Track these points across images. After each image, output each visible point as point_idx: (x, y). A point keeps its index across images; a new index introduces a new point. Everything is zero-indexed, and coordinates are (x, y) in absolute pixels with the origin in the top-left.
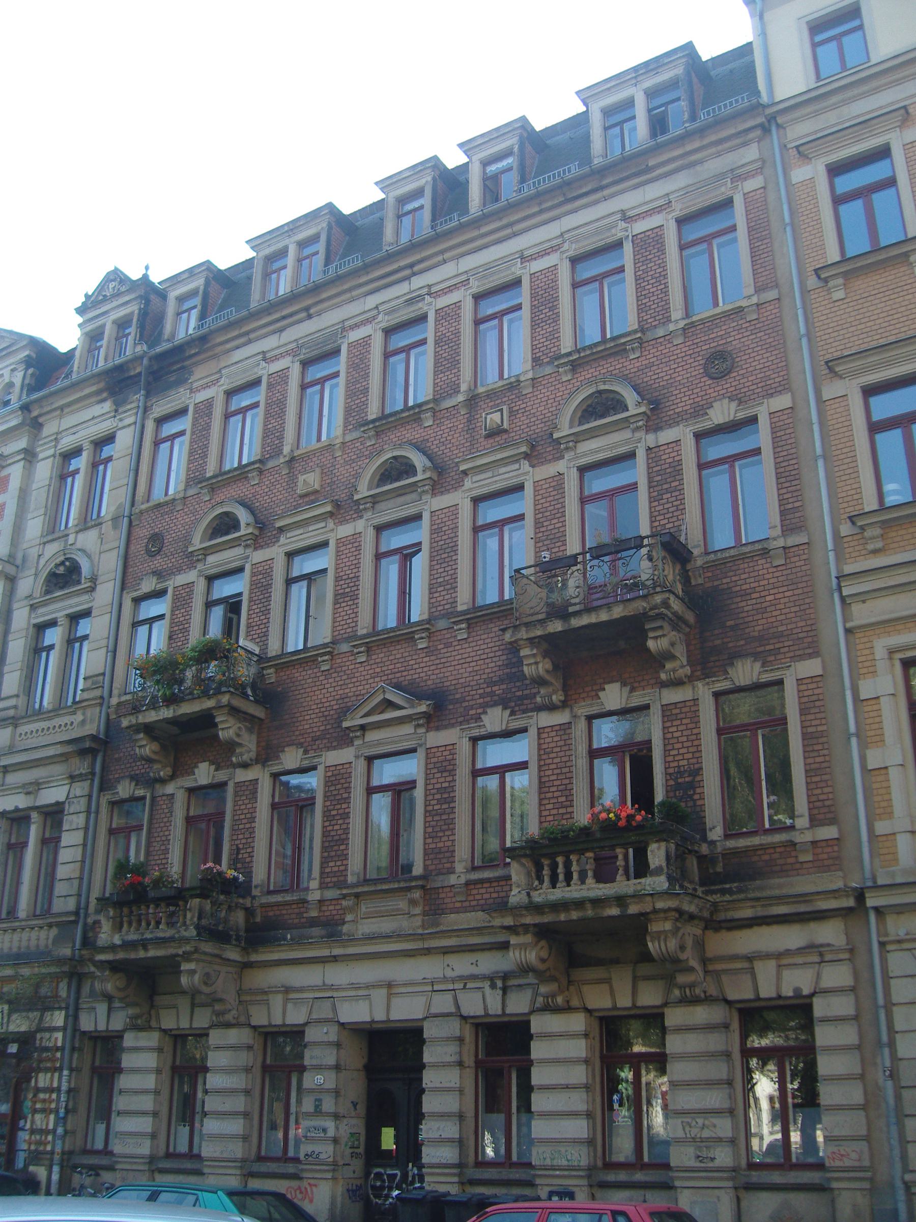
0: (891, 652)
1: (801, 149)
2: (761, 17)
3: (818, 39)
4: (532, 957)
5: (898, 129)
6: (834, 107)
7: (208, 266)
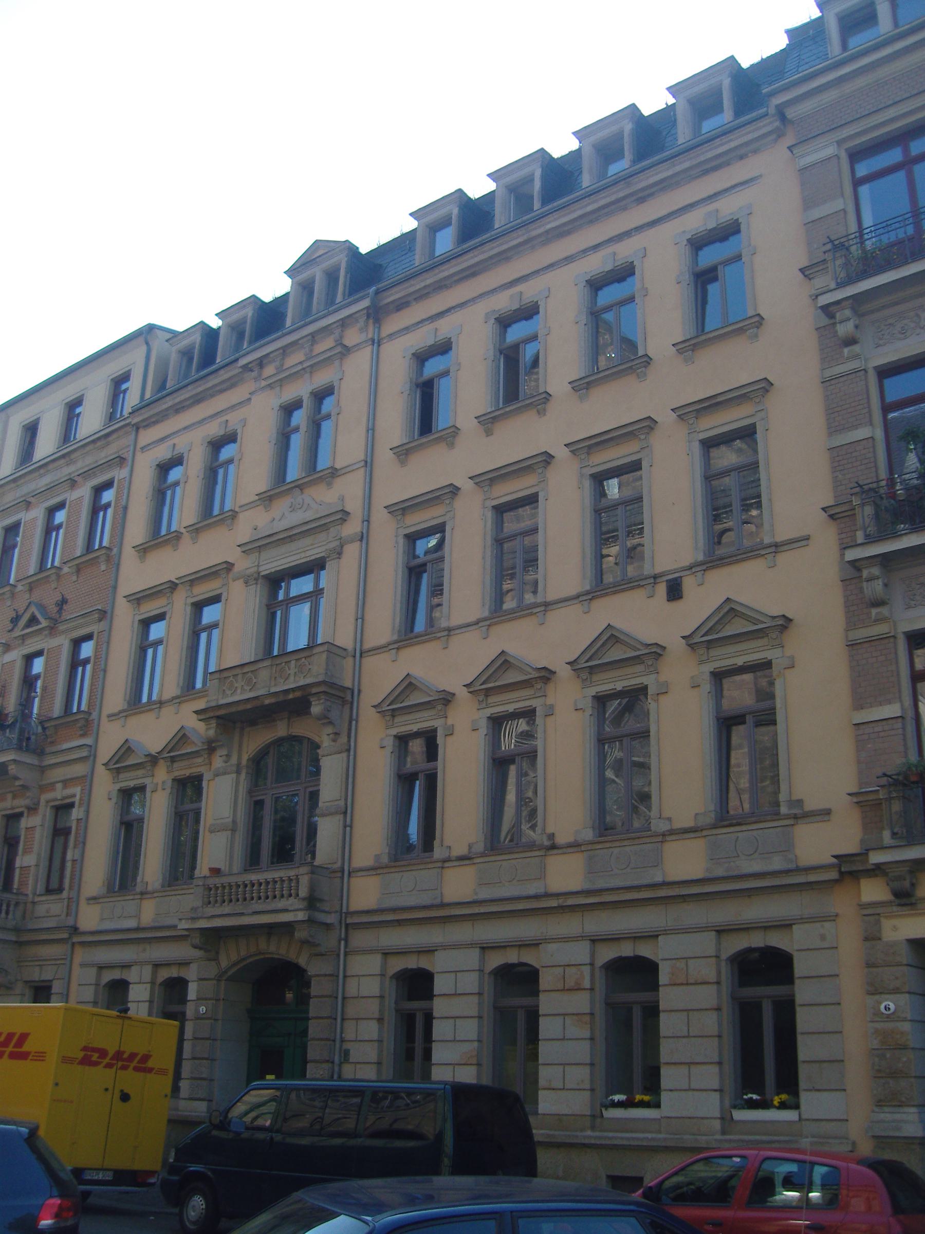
7: (254, 299)
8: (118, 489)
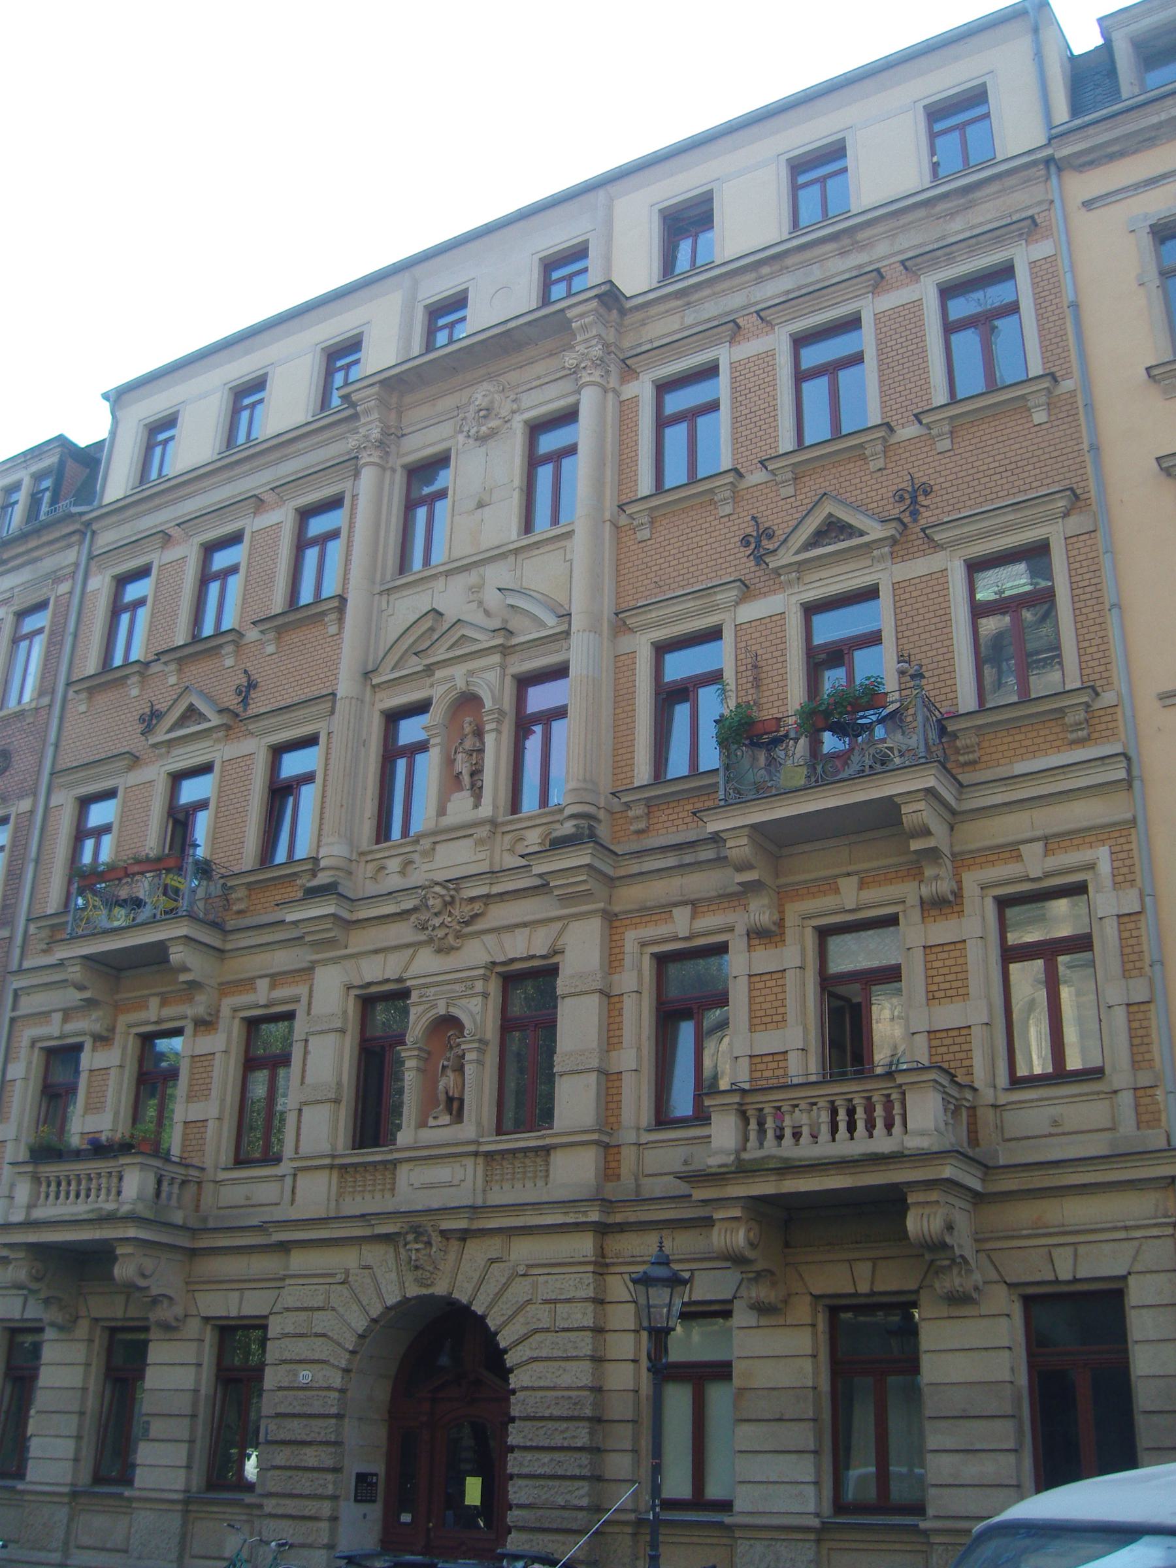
3: (938, 127)
4: (739, 1238)
5: (870, 295)
7: (62, 442)
8: (158, 579)
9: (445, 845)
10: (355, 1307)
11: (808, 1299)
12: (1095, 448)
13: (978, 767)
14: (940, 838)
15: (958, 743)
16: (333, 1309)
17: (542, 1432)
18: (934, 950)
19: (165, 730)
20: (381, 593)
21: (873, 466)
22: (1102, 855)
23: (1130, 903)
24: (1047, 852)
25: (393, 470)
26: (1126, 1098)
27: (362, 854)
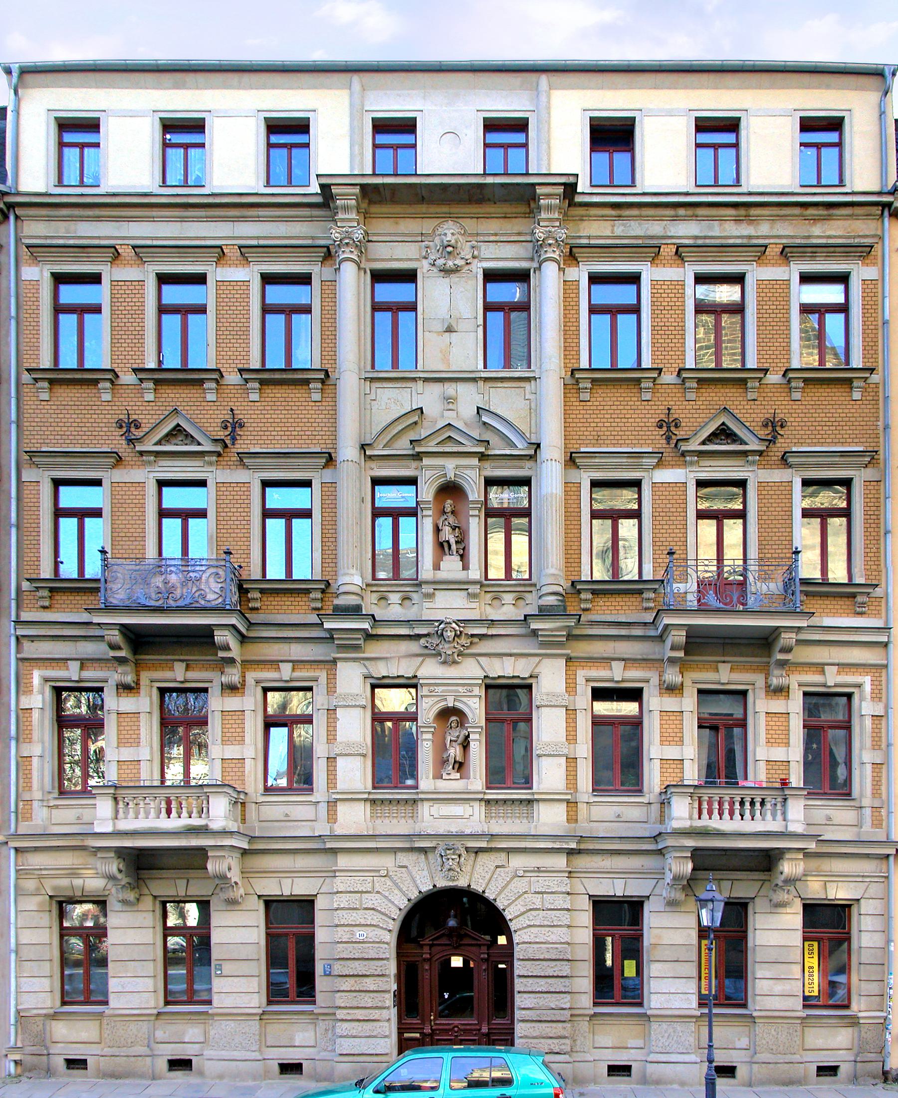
0: (257, 682)
1: (574, 250)
2: (16, 92)
6: (64, 219)
9: (443, 592)
10: (396, 892)
11: (151, 898)
12: (886, 427)
13: (260, 611)
14: (235, 651)
15: (249, 595)
16: (378, 892)
17: (539, 967)
18: (123, 716)
19: (153, 442)
20: (365, 379)
21: (751, 396)
22: (867, 681)
23: (879, 710)
24: (839, 673)
25: (365, 272)
26: (868, 812)
27: (368, 585)
